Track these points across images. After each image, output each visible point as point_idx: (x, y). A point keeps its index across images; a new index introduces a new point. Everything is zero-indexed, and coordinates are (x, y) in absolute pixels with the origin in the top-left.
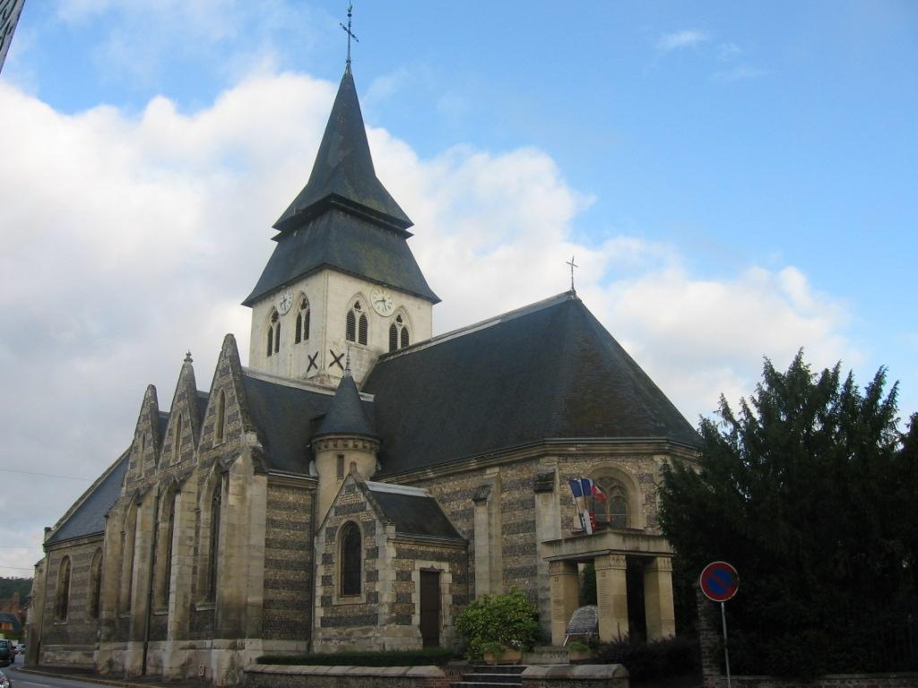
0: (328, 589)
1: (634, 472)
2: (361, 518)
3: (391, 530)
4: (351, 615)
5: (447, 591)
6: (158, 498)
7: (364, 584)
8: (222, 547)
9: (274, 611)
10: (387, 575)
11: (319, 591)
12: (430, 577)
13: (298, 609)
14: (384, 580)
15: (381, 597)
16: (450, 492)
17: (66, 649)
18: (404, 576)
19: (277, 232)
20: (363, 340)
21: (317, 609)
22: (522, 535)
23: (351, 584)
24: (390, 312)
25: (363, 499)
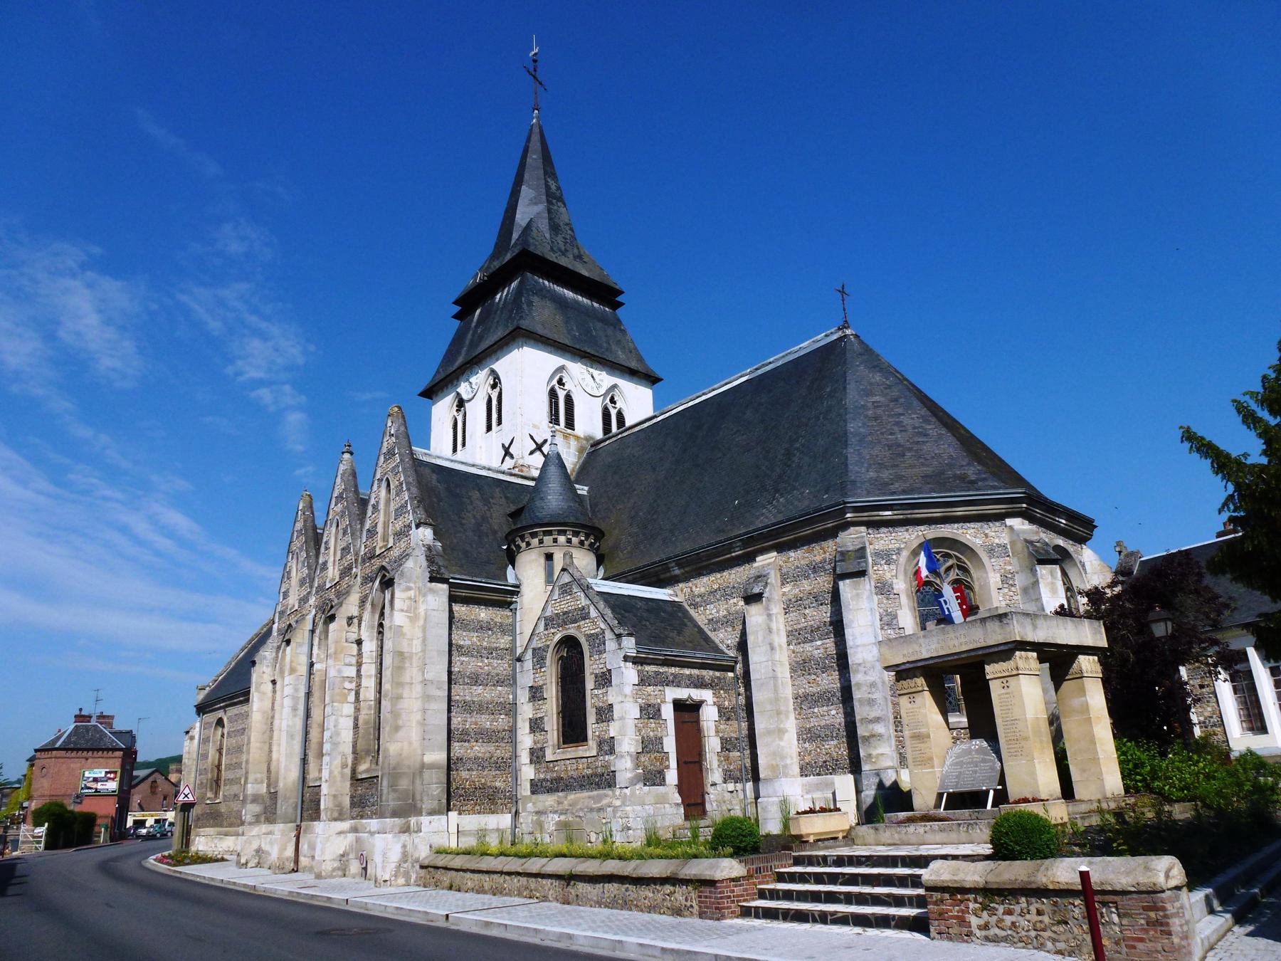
0: (540, 737)
1: (979, 541)
2: (581, 631)
3: (629, 644)
4: (575, 774)
5: (712, 732)
6: (313, 631)
7: (592, 727)
8: (386, 686)
9: (464, 774)
10: (626, 708)
11: (526, 740)
12: (687, 710)
13: (498, 768)
14: (622, 718)
15: (620, 745)
16: (705, 598)
17: (219, 834)
18: (650, 712)
19: (458, 308)
20: (570, 423)
21: (524, 768)
22: (819, 643)
23: (573, 730)
24: (603, 391)
25: (584, 601)
